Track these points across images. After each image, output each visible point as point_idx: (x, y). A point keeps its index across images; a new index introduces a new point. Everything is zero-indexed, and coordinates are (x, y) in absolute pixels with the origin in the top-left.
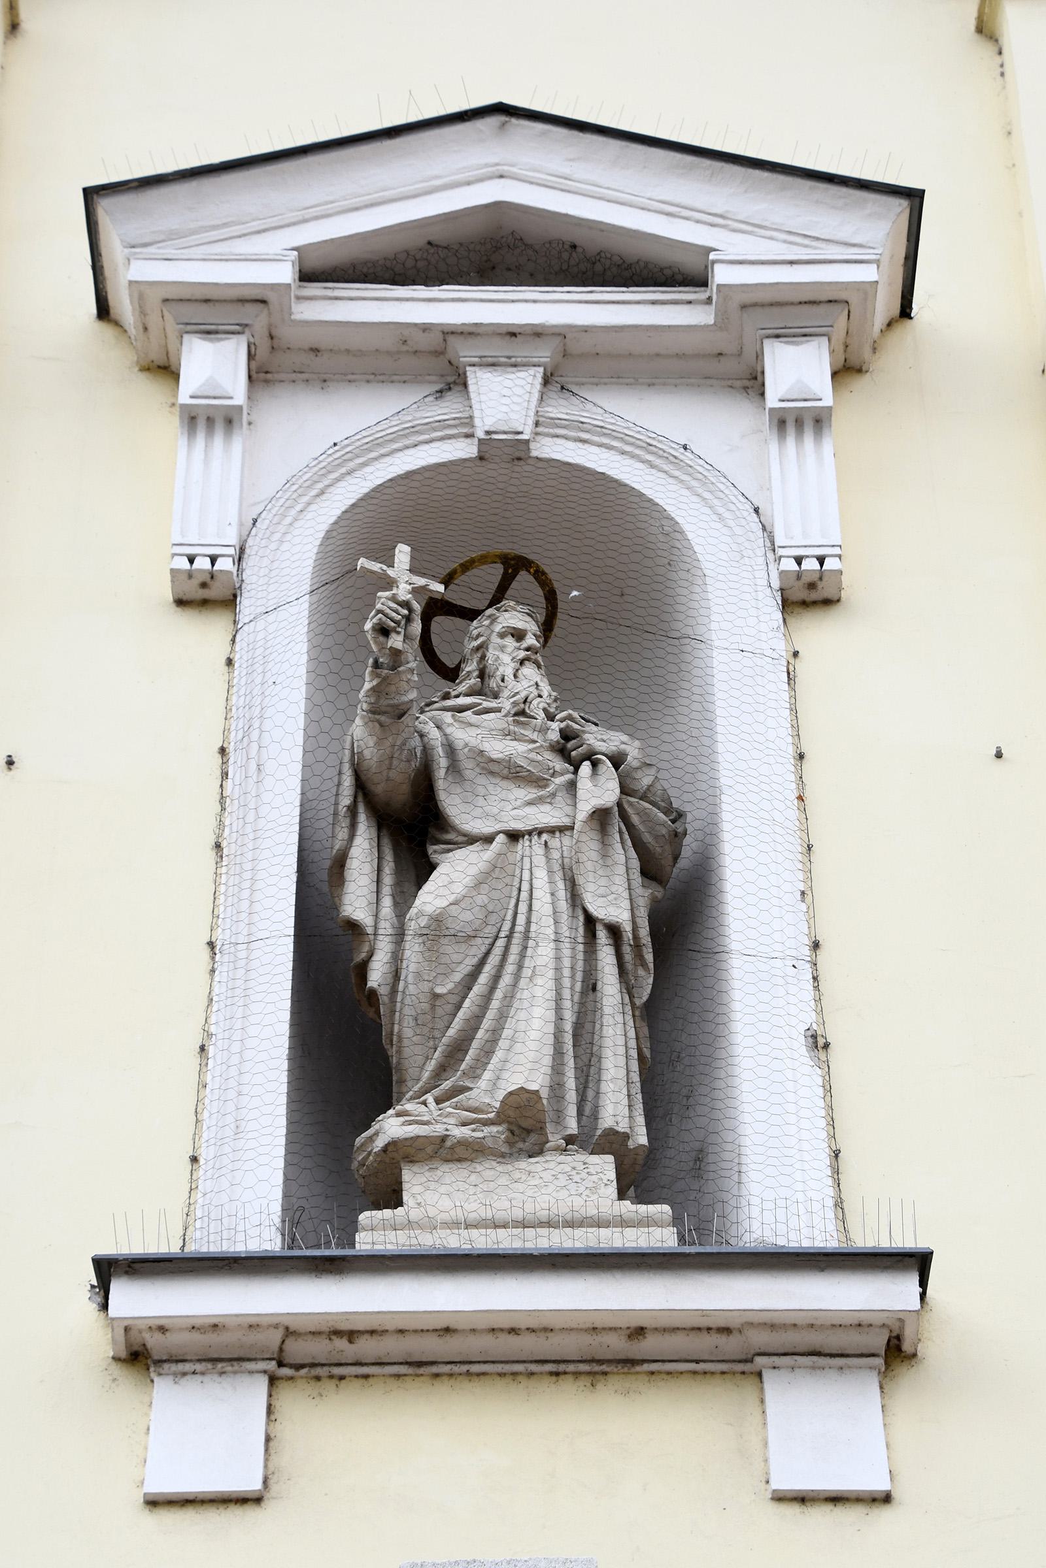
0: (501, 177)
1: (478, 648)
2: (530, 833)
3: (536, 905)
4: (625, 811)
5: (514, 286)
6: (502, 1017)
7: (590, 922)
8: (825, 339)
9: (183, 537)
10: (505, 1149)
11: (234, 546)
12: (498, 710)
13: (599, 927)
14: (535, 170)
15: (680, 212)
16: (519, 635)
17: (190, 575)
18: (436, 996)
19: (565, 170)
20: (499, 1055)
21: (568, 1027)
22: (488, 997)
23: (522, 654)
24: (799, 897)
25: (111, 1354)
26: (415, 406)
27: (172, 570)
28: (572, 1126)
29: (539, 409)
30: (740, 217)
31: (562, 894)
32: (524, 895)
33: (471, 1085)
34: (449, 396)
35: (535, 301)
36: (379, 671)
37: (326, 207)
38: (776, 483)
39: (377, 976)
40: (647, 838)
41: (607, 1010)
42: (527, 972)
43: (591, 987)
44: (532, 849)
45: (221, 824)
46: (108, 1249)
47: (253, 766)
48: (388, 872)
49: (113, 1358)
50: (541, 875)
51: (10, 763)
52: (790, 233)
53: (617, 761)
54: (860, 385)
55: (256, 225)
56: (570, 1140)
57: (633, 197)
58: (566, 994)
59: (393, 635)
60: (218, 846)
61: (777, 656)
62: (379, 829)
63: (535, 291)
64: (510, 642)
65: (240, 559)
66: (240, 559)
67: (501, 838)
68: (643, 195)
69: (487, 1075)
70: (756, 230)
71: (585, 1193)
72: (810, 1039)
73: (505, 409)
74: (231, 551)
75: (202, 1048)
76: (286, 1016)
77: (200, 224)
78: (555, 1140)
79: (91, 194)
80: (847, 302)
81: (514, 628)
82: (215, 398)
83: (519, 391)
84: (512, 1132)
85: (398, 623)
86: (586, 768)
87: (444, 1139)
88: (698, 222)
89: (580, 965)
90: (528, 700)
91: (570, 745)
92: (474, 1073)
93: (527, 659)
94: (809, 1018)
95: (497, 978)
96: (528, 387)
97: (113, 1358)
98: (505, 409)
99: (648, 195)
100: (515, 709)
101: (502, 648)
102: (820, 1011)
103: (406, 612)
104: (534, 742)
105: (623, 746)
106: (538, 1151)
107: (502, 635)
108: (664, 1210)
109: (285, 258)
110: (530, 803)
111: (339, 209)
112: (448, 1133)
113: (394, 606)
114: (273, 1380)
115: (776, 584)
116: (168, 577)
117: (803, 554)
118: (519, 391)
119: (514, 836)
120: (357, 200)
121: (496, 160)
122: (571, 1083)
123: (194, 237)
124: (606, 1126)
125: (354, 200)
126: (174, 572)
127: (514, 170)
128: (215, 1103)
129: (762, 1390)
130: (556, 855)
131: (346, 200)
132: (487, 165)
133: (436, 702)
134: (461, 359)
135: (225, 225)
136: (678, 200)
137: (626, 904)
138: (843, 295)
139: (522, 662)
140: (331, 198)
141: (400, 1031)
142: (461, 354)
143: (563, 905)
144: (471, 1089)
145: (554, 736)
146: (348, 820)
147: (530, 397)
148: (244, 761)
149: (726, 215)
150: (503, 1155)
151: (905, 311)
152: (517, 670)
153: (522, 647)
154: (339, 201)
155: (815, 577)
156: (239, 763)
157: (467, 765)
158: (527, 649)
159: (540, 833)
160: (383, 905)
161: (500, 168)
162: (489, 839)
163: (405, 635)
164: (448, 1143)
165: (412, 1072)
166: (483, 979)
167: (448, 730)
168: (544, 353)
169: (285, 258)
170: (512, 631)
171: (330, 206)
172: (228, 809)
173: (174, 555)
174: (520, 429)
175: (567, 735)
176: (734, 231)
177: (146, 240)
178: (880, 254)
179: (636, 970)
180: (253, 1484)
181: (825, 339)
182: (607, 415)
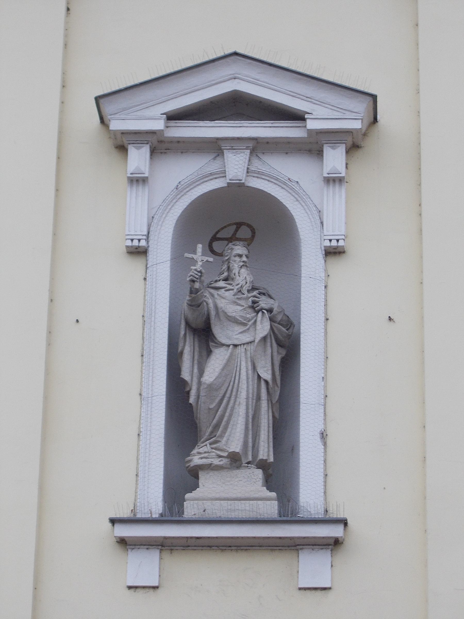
0: (235, 78)
1: (227, 260)
2: (241, 345)
3: (241, 376)
4: (273, 328)
5: (240, 121)
6: (231, 415)
7: (259, 377)
8: (344, 145)
9: (129, 231)
10: (229, 467)
11: (145, 235)
12: (233, 290)
13: (262, 380)
14: (247, 77)
15: (296, 96)
16: (240, 256)
17: (132, 247)
18: (210, 409)
19: (258, 77)
20: (229, 430)
21: (251, 416)
22: (225, 412)
23: (242, 264)
24: (321, 380)
25: (116, 541)
26: (206, 165)
27: (126, 246)
28: (250, 459)
29: (249, 167)
30: (316, 99)
31: (250, 367)
32: (238, 369)
33: (220, 440)
34: (218, 158)
35: (247, 127)
36: (191, 295)
37: (176, 94)
38: (325, 202)
39: (192, 400)
40: (280, 336)
41: (263, 413)
42: (237, 403)
43: (259, 398)
44: (241, 350)
45: (143, 349)
46: (113, 516)
47: (152, 328)
48: (196, 354)
49: (117, 542)
50: (243, 364)
51: (77, 321)
52: (333, 106)
53: (270, 311)
54: (359, 154)
55: (151, 103)
56: (248, 463)
57: (280, 89)
58: (250, 407)
59: (196, 283)
60: (140, 395)
61: (321, 279)
62: (194, 335)
63: (247, 123)
64: (237, 259)
65: (147, 240)
66: (147, 240)
67: (231, 347)
68: (283, 88)
69: (225, 439)
70: (322, 104)
71: (253, 483)
72: (321, 435)
73: (236, 171)
74: (145, 237)
75: (139, 435)
76: (164, 418)
77: (133, 104)
78: (244, 461)
79: (97, 99)
80: (352, 132)
81: (239, 254)
82: (139, 174)
83: (241, 162)
84: (232, 461)
85: (197, 279)
86: (260, 314)
87: (211, 464)
88: (302, 99)
89: (255, 390)
90: (242, 286)
91: (255, 305)
92: (222, 436)
93: (243, 265)
94: (322, 427)
95: (230, 397)
96: (244, 160)
97: (117, 542)
98: (236, 171)
99: (286, 88)
100: (238, 291)
101: (235, 261)
102: (325, 424)
103: (200, 274)
104: (244, 306)
105: (272, 306)
106: (239, 467)
107: (235, 256)
108: (274, 494)
109: (161, 118)
110: (241, 333)
111: (180, 95)
112: (212, 463)
113: (196, 273)
114: (161, 550)
115: (323, 248)
116: (125, 247)
117: (332, 238)
118: (241, 162)
119: (235, 346)
120: (187, 91)
121: (234, 73)
122: (250, 440)
123: (131, 109)
124: (261, 458)
125: (185, 91)
126: (127, 247)
127: (239, 76)
128: (142, 474)
129: (298, 552)
130: (249, 353)
131: (182, 91)
132: (231, 75)
133: (213, 284)
134: (222, 148)
135: (142, 104)
136: (295, 91)
137: (270, 372)
138: (352, 131)
139: (241, 267)
140: (176, 91)
141: (199, 416)
142: (222, 146)
143: (250, 372)
144: (220, 441)
145: (250, 304)
146: (183, 339)
147: (244, 168)
148: (150, 322)
149: (311, 98)
150: (229, 468)
151: (375, 120)
152: (240, 270)
153: (242, 260)
154: (180, 92)
155: (336, 247)
156: (148, 327)
157: (221, 314)
158: (243, 262)
159: (244, 344)
160: (195, 367)
161: (235, 75)
162: (228, 346)
163: (200, 281)
164: (212, 466)
165: (204, 429)
166: (225, 401)
167: (216, 300)
168: (251, 145)
169: (161, 118)
170: (238, 255)
171: (177, 94)
172: (145, 343)
173: (126, 239)
174: (241, 179)
175: (254, 302)
176: (314, 104)
177: (116, 112)
178: (362, 116)
179: (274, 387)
180: (157, 585)
181: (344, 145)
182: (271, 169)
